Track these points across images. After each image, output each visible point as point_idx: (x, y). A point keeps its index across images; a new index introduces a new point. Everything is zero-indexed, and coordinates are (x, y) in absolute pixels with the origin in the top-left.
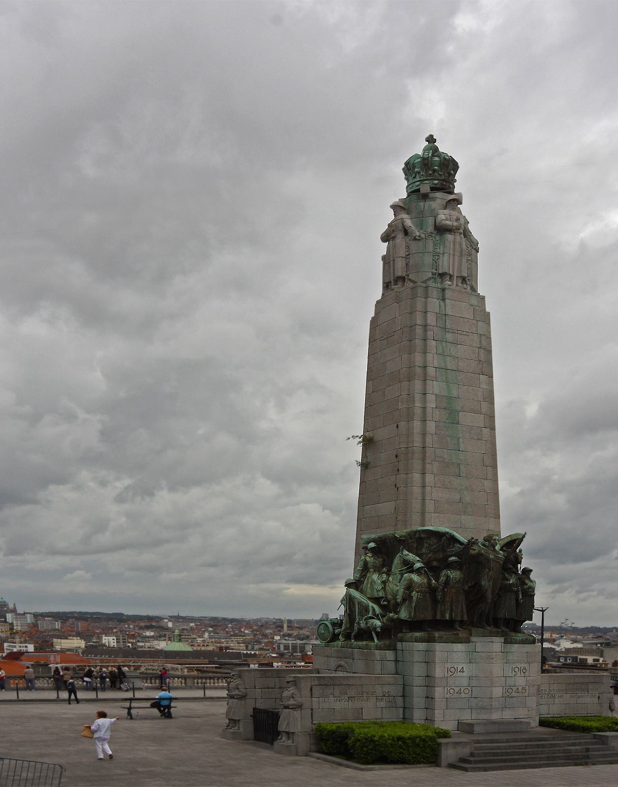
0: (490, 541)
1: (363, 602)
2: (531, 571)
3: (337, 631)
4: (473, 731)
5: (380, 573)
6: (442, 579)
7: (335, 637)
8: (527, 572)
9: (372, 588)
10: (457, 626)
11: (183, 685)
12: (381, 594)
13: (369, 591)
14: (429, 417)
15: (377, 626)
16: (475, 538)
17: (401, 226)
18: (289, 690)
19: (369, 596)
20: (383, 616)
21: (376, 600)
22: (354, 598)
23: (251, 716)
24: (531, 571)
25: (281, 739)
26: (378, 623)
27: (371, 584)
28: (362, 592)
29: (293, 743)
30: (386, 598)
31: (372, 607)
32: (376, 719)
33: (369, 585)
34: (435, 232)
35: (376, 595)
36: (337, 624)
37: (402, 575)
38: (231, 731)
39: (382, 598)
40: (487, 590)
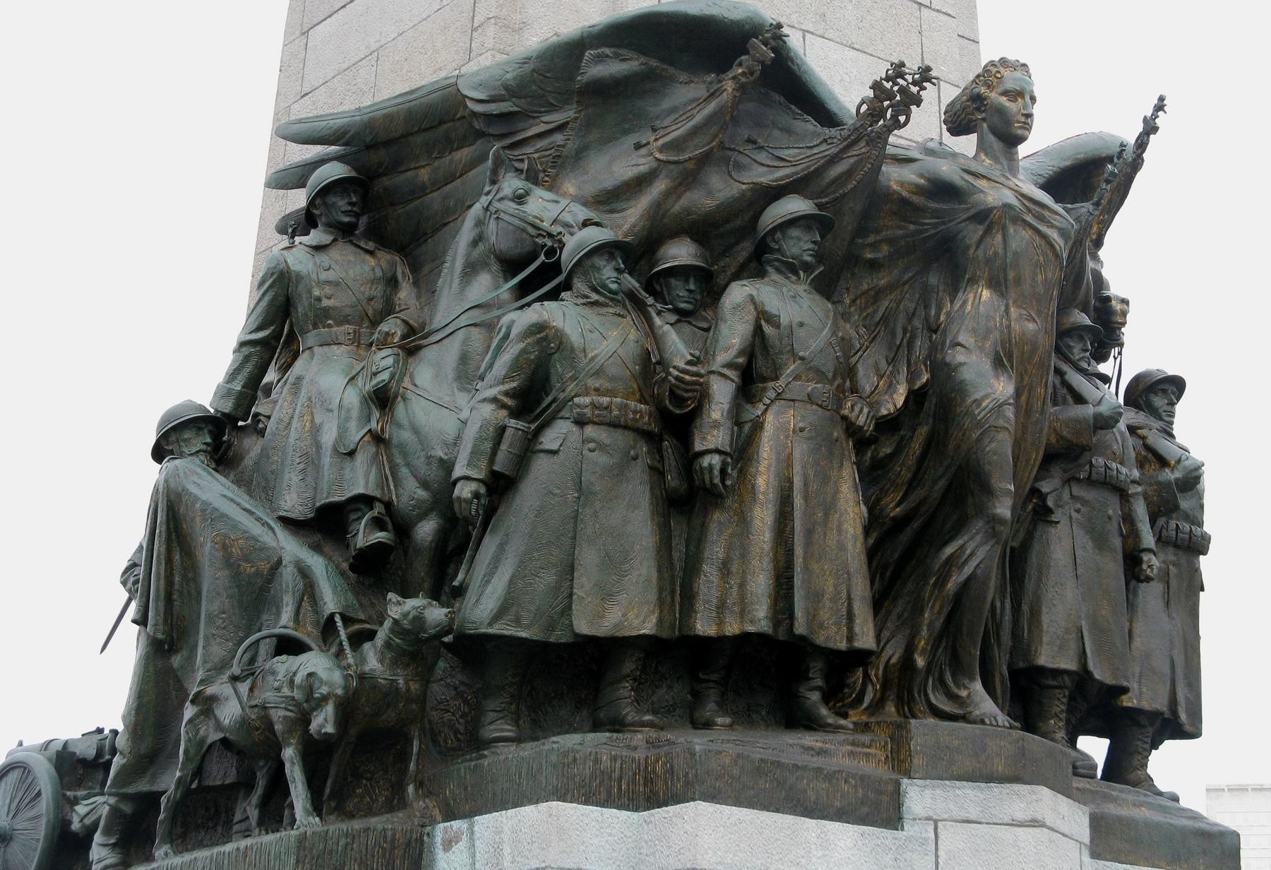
0: (992, 111)
2: (1174, 386)
5: (362, 344)
6: (733, 334)
8: (1156, 393)
10: (815, 697)
12: (361, 479)
16: (912, 65)
20: (359, 639)
24: (1174, 386)
28: (259, 485)
30: (388, 505)
31: (304, 572)
39: (365, 501)
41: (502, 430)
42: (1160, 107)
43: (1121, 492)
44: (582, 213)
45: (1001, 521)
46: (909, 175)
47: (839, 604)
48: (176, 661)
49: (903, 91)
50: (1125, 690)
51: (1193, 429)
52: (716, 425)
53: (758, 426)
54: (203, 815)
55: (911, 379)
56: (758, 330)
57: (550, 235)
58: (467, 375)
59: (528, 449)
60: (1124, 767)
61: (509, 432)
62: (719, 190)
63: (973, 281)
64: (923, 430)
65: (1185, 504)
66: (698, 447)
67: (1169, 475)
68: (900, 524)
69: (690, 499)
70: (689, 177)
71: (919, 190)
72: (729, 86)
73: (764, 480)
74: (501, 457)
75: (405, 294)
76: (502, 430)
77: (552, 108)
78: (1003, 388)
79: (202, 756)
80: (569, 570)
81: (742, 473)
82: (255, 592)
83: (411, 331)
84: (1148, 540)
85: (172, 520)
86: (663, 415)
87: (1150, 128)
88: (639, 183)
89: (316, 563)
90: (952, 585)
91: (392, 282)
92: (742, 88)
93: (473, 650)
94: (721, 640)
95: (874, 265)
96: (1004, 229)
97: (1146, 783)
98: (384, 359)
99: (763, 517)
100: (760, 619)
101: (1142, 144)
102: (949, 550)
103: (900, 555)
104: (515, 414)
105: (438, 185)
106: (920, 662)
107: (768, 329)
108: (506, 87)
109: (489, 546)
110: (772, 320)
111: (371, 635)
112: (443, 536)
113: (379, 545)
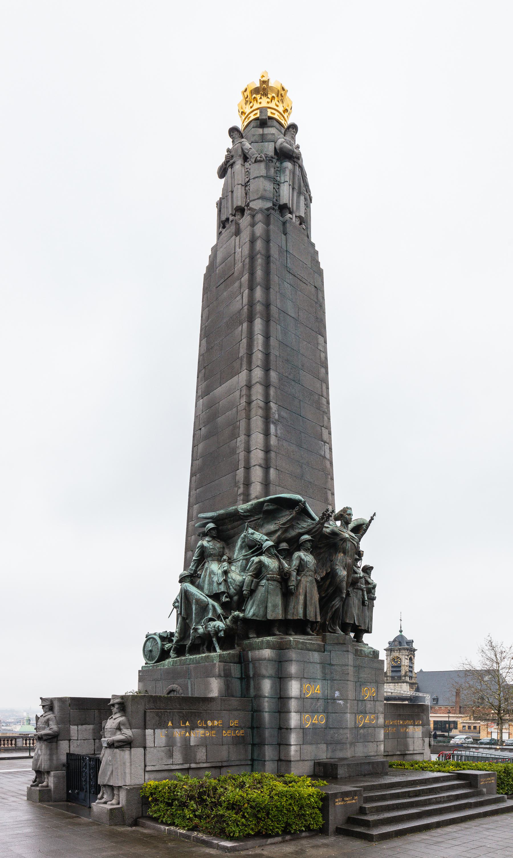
1: (201, 599)
2: (372, 568)
3: (167, 646)
4: (337, 774)
6: (295, 563)
7: (164, 655)
8: (368, 570)
9: (211, 583)
11: (13, 746)
12: (222, 588)
13: (206, 586)
14: (272, 366)
15: (221, 629)
17: (240, 152)
18: (114, 718)
19: (207, 592)
20: (225, 618)
21: (216, 597)
22: (192, 594)
23: (64, 765)
24: (372, 568)
25: (102, 798)
26: (220, 624)
27: (210, 575)
28: (200, 588)
29: (119, 804)
30: (228, 593)
31: (213, 606)
32: (222, 762)
33: (207, 579)
34: (276, 158)
35: (216, 589)
36: (166, 638)
37: (248, 560)
38: (38, 788)
39: (223, 593)
40: (342, 581)
41: (252, 581)
42: (374, 515)
43: (362, 590)
44: (266, 538)
45: (343, 598)
46: (328, 530)
47: (314, 613)
48: (187, 621)
49: (328, 514)
50: (360, 626)
51: (374, 577)
52: (293, 580)
53: (300, 580)
54: (195, 649)
55: (326, 570)
56: (300, 562)
57: (259, 542)
58: (244, 569)
59: (258, 584)
60: (358, 638)
61: (254, 582)
62: (293, 533)
63: (340, 552)
64: (329, 580)
65: (373, 591)
66: (290, 584)
67: (370, 586)
68: (324, 597)
69: (287, 594)
70: (286, 531)
71: (329, 533)
72: (294, 512)
73: (301, 590)
74: (252, 586)
75: (227, 551)
76: (252, 581)
77: (258, 515)
78: (345, 573)
79: (195, 638)
80: (266, 607)
81: (297, 589)
82: (203, 608)
83: (229, 559)
84: (366, 599)
85: (185, 595)
86: (282, 578)
87: (372, 519)
88: (275, 532)
89: (216, 604)
90: (334, 609)
91: (224, 548)
92: (296, 513)
93: (245, 620)
94: (294, 620)
95: (320, 548)
96: (346, 542)
97: (362, 642)
98: (225, 564)
99: (302, 598)
100: (301, 616)
101: (370, 522)
102: (333, 603)
103: (324, 603)
104: (255, 578)
105: (233, 528)
106: (327, 623)
107: (302, 562)
108: (247, 510)
109: (250, 603)
110: (303, 560)
111: (228, 618)
112: (239, 599)
113: (227, 601)
